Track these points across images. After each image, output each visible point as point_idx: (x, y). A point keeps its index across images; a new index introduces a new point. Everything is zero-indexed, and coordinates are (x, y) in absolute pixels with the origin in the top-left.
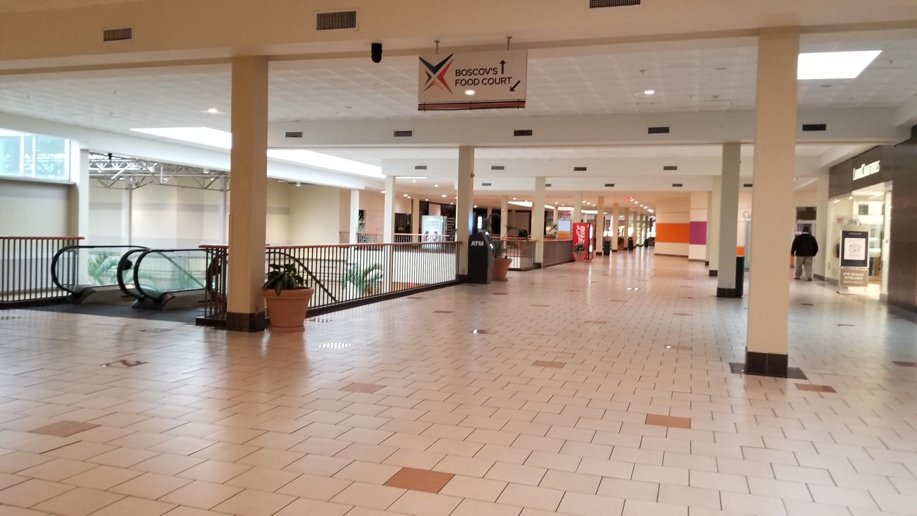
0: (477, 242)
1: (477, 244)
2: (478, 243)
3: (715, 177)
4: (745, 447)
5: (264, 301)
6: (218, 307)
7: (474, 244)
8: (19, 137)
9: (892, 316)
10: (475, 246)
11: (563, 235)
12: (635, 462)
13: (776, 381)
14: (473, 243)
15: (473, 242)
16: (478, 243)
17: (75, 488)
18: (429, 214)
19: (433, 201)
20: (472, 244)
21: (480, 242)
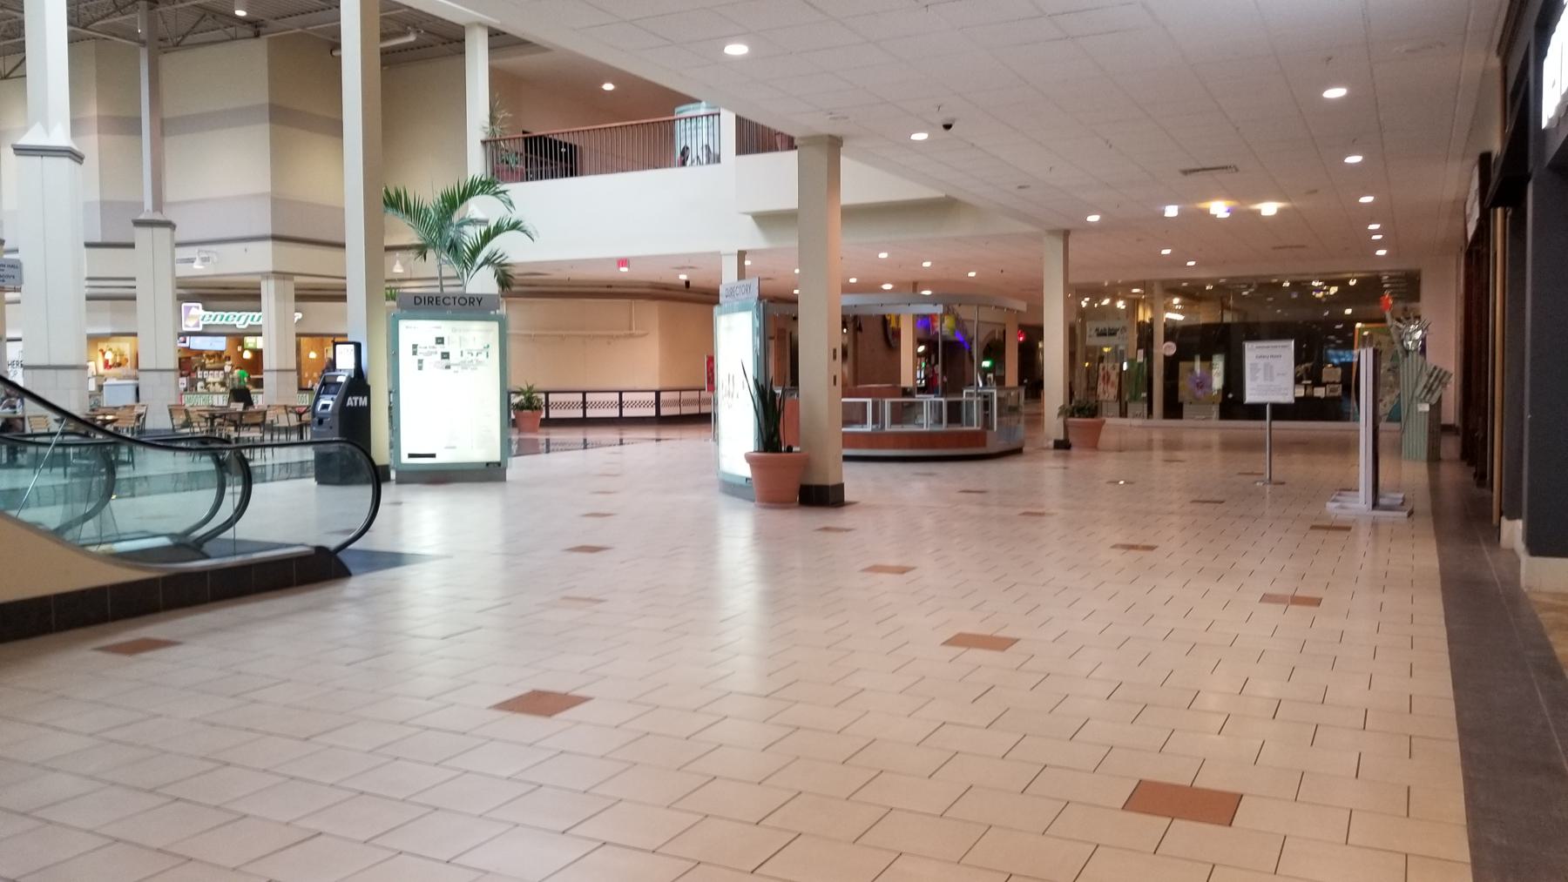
0: (356, 399)
1: (356, 404)
2: (358, 402)
3: (256, 196)
4: (1414, 855)
5: (860, 389)
6: (1238, 286)
7: (352, 404)
8: (865, 404)
9: (761, 504)
10: (354, 407)
11: (228, 345)
12: (1098, 842)
13: (661, 278)
14: (350, 402)
15: (350, 399)
16: (358, 402)
17: (555, 756)
18: (1184, 416)
19: (589, 389)
20: (348, 404)
21: (361, 398)
